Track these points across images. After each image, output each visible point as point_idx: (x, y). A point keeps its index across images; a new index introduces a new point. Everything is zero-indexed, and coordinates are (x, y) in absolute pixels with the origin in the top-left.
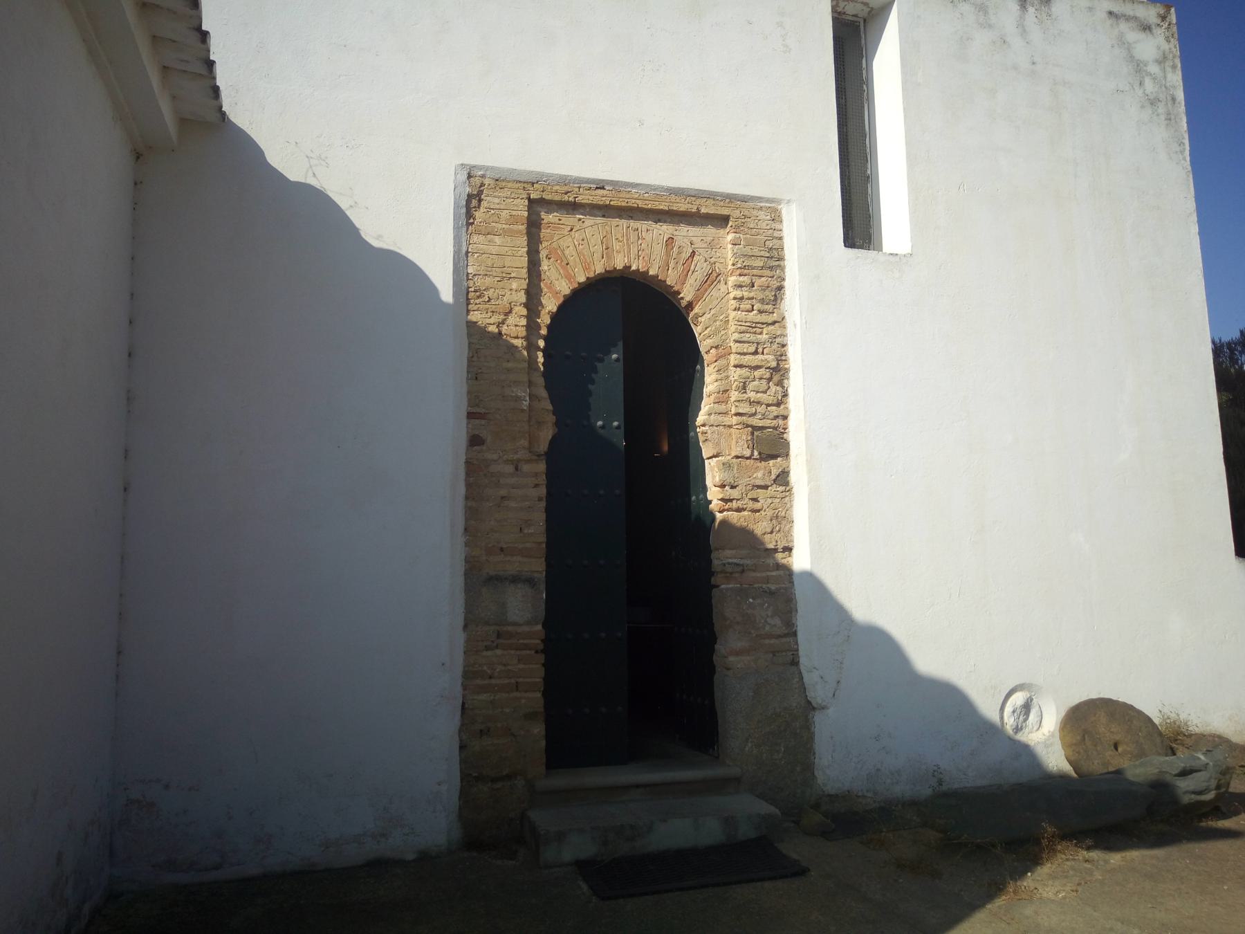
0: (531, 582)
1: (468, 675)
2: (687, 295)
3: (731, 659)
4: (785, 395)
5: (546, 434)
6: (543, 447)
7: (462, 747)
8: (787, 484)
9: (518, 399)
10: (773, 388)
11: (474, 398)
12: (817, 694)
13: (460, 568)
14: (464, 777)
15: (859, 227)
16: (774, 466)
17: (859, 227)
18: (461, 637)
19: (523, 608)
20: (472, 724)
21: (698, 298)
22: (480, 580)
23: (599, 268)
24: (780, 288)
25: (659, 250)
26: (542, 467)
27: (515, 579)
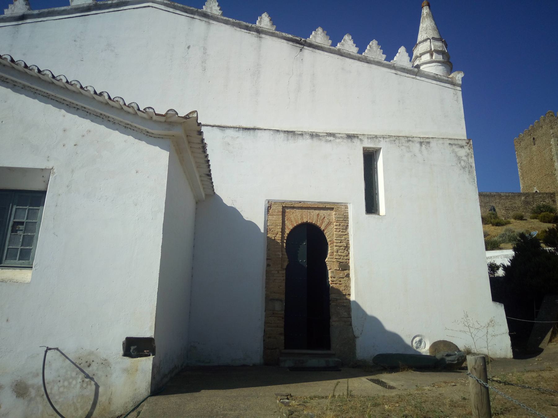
0: (281, 300)
1: (266, 323)
2: (322, 228)
3: (333, 323)
4: (349, 253)
5: (286, 264)
6: (285, 267)
7: (264, 340)
8: (349, 277)
9: (279, 255)
10: (345, 252)
11: (268, 255)
12: (357, 333)
13: (264, 296)
14: (265, 348)
15: (371, 206)
16: (346, 272)
17: (371, 206)
18: (264, 313)
19: (279, 307)
20: (267, 335)
21: (325, 229)
22: (269, 300)
23: (300, 222)
24: (348, 226)
25: (315, 217)
26: (284, 272)
27: (277, 300)
